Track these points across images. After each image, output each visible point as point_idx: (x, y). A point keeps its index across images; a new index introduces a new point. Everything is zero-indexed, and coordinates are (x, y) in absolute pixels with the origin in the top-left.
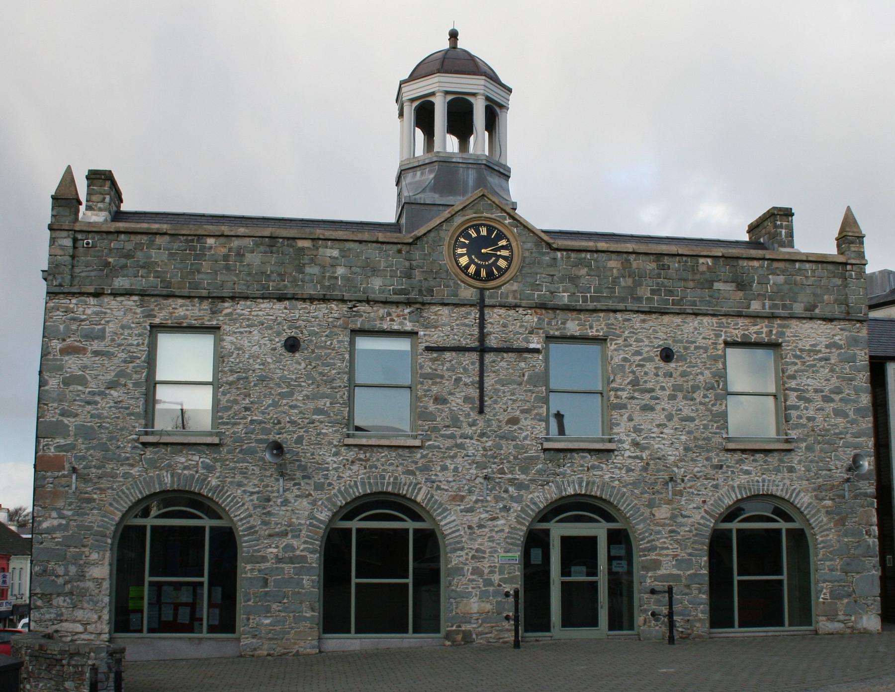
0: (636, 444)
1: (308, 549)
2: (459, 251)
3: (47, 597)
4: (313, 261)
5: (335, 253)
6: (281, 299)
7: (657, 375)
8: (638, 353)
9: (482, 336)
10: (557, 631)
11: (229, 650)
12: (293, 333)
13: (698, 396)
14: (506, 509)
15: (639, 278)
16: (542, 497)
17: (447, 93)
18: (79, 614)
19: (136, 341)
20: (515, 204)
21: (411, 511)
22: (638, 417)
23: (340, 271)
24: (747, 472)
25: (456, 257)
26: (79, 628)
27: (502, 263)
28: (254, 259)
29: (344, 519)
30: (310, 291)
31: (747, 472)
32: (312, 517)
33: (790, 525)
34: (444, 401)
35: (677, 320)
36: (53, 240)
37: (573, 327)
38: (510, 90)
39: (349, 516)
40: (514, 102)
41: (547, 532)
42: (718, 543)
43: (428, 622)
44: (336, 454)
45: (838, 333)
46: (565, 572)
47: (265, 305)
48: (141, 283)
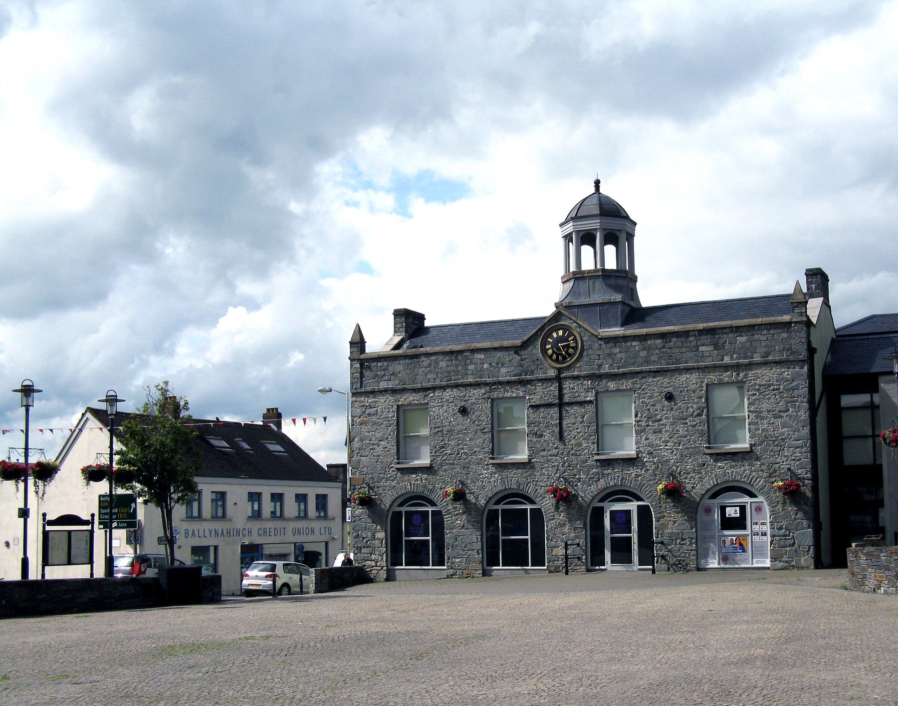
0: (650, 453)
2: (548, 347)
5: (482, 356)
6: (457, 386)
8: (651, 397)
9: (561, 396)
10: (608, 565)
17: (604, 229)
22: (652, 437)
23: (485, 366)
26: (373, 563)
30: (471, 380)
36: (351, 365)
38: (635, 224)
39: (498, 502)
43: (539, 560)
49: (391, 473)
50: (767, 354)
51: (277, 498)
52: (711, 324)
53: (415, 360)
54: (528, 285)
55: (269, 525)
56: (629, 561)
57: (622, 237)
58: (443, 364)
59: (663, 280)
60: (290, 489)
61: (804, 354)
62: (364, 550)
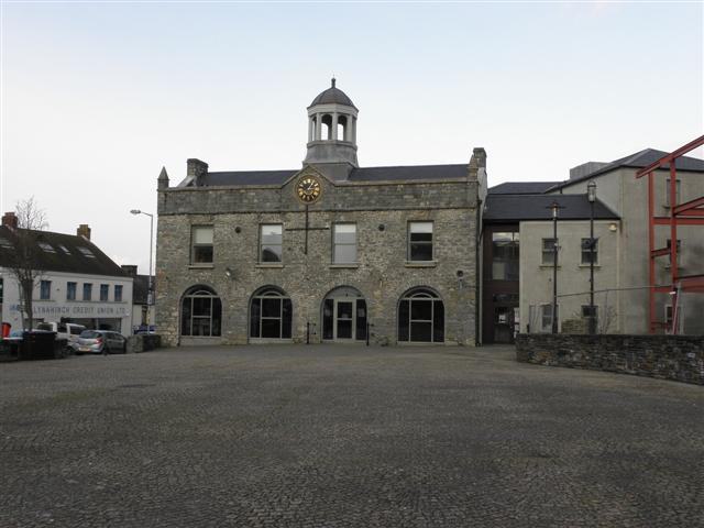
1: (244, 305)
3: (159, 323)
6: (234, 213)
9: (307, 224)
10: (335, 339)
11: (218, 342)
13: (395, 245)
15: (371, 195)
19: (187, 231)
21: (283, 293)
25: (298, 192)
27: (316, 194)
28: (225, 198)
30: (244, 210)
35: (387, 213)
37: (342, 219)
40: (359, 116)
42: (403, 305)
43: (287, 334)
45: (461, 214)
46: (339, 316)
47: (229, 216)
48: (187, 210)
49: (184, 271)
50: (450, 203)
51: (88, 287)
52: (413, 181)
53: (197, 196)
54: (281, 147)
55: (82, 305)
56: (350, 337)
57: (350, 120)
58: (225, 198)
59: (376, 149)
60: (97, 281)
61: (475, 203)
62: (163, 324)
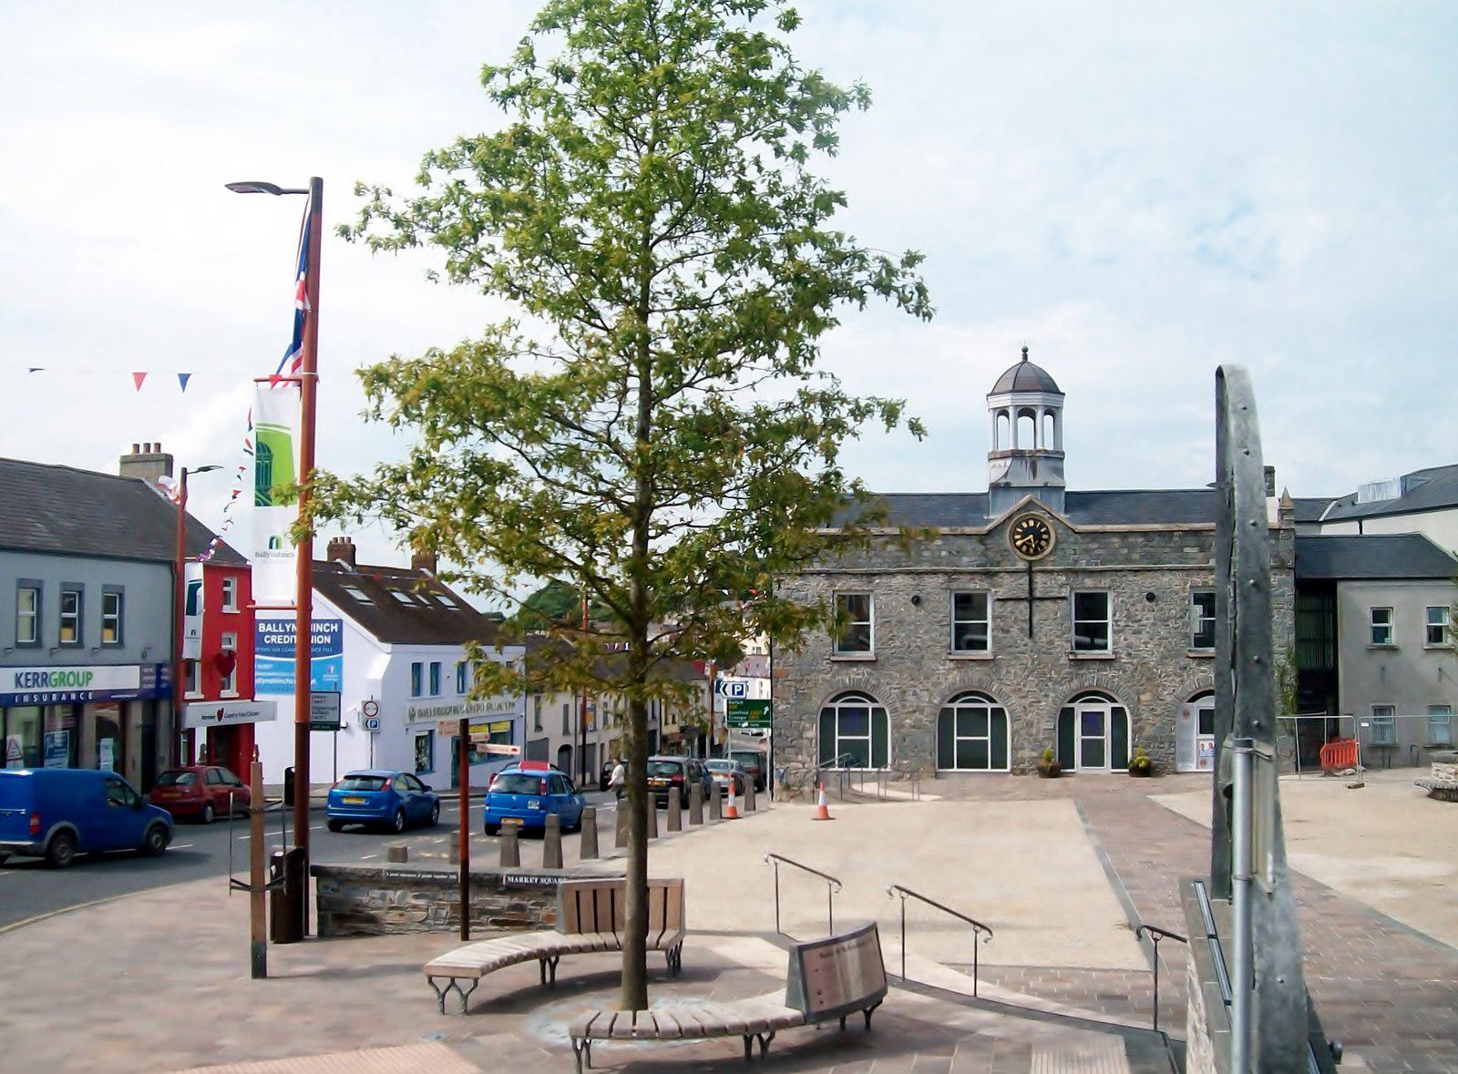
0: (1129, 655)
1: (929, 720)
4: (926, 549)
7: (1143, 610)
8: (1132, 597)
9: (1031, 590)
12: (916, 593)
14: (1046, 696)
16: (1067, 689)
18: (800, 758)
20: (431, 353)
22: (1132, 639)
24: (1203, 671)
29: (1070, 702)
30: (925, 568)
31: (1203, 671)
32: (930, 702)
33: (994, 706)
34: (1008, 631)
41: (1073, 709)
44: (944, 665)
